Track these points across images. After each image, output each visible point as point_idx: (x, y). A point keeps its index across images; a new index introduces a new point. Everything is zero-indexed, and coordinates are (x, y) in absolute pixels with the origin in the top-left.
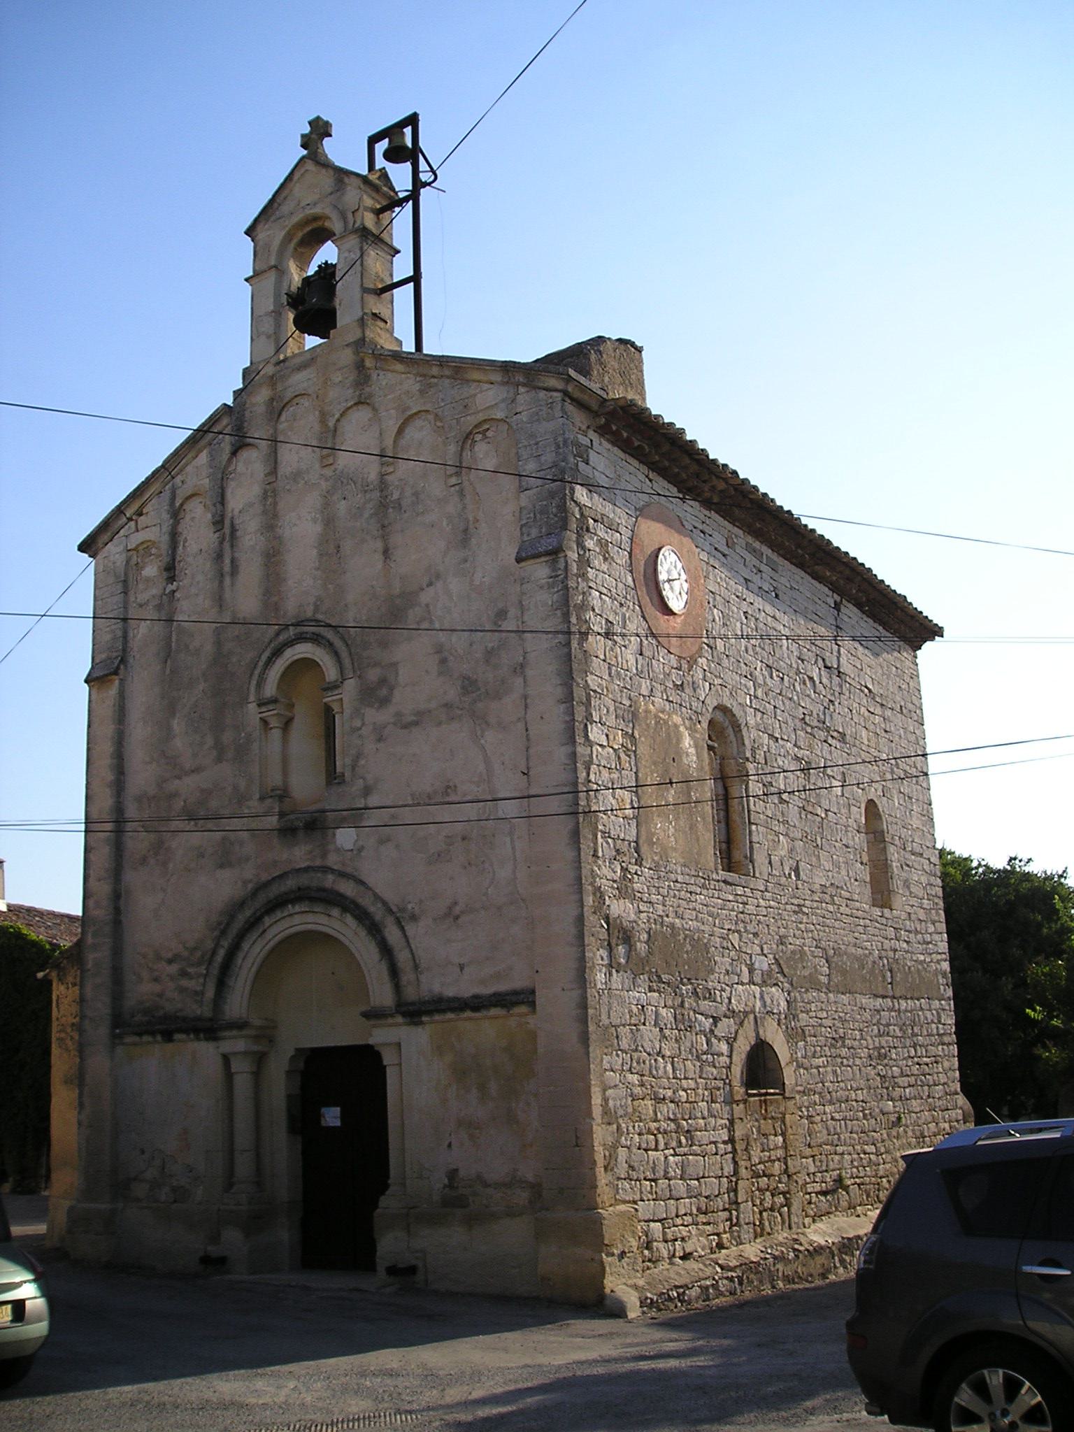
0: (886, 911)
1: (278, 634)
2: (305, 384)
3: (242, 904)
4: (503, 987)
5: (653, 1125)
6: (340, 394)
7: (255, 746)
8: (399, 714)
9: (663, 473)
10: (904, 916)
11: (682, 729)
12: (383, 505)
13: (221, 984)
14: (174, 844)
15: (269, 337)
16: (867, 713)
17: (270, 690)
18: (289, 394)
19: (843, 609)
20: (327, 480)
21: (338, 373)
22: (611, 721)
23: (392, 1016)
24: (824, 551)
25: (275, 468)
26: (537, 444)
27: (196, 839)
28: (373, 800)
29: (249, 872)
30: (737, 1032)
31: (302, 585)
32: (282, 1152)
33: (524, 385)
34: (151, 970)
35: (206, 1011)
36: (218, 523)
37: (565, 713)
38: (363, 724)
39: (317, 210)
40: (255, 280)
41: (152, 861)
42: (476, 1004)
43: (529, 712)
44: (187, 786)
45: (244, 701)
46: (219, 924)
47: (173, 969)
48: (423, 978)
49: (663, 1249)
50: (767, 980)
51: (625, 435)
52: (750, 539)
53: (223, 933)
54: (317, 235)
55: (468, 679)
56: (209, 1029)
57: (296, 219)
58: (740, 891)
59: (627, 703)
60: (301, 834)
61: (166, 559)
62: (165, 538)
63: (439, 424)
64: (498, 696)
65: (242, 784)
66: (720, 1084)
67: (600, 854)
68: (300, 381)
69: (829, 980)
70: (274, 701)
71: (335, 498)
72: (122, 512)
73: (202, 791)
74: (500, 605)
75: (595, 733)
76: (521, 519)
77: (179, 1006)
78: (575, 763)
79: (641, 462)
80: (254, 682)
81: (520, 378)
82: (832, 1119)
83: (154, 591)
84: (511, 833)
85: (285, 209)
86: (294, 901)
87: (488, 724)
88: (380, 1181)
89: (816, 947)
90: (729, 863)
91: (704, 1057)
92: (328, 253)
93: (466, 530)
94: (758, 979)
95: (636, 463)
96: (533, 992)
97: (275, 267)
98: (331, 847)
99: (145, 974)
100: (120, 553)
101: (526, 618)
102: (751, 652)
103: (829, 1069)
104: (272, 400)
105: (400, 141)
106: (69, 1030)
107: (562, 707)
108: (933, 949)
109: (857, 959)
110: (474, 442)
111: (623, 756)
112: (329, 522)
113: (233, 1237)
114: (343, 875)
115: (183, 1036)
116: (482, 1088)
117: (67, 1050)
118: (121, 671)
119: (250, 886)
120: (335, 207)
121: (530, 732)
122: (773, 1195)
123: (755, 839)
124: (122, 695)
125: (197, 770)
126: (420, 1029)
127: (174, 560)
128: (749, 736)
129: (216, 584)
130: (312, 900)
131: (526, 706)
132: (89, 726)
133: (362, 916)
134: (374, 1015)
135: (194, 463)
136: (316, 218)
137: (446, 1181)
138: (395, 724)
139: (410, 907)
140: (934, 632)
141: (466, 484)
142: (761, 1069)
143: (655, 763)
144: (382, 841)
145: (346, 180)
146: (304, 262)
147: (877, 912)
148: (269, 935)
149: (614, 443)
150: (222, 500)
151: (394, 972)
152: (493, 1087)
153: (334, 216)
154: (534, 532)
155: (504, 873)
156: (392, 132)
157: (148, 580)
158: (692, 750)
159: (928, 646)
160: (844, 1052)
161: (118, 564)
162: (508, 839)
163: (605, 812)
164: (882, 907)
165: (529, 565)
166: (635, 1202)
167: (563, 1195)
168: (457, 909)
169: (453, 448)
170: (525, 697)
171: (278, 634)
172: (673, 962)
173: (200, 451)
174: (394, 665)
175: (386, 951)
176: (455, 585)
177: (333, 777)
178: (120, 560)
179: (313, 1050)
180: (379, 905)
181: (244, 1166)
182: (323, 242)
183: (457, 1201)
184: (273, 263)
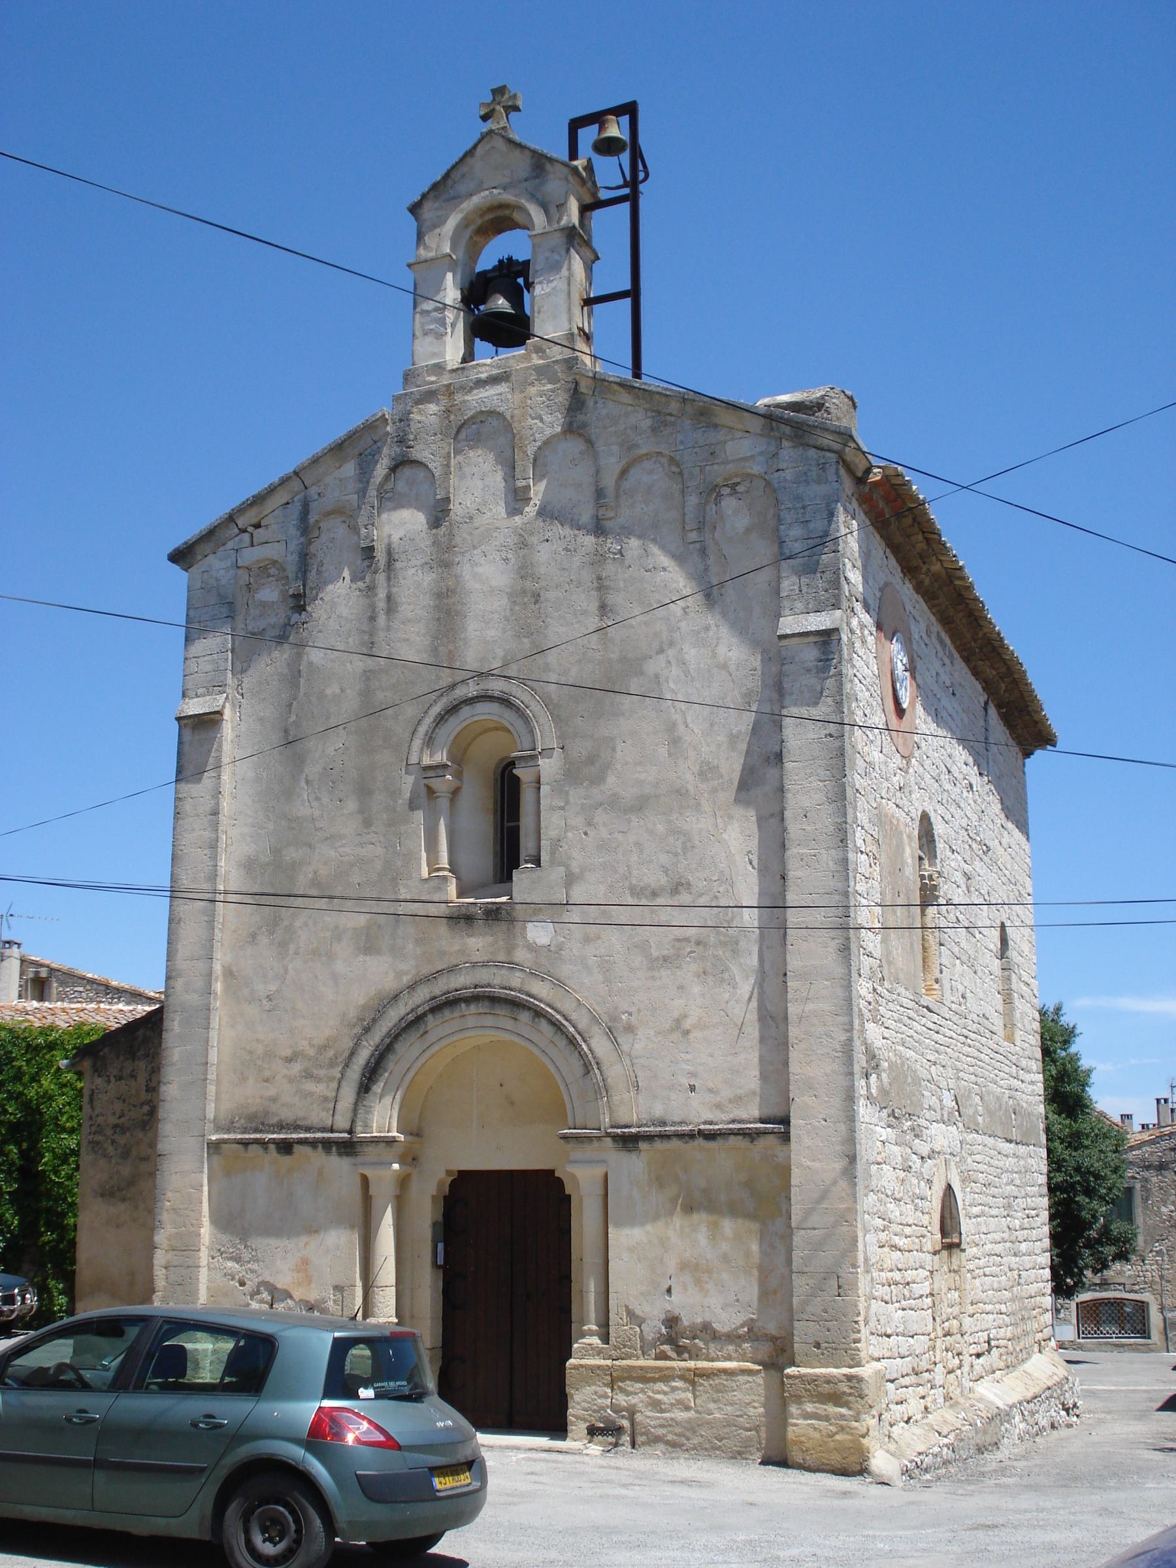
26: (804, 508)
28: (578, 894)
77: (301, 1114)
83: (273, 620)
100: (227, 569)
106: (109, 1132)
110: (720, 495)
126: (634, 1156)
144: (587, 940)
145: (548, 167)
157: (264, 605)
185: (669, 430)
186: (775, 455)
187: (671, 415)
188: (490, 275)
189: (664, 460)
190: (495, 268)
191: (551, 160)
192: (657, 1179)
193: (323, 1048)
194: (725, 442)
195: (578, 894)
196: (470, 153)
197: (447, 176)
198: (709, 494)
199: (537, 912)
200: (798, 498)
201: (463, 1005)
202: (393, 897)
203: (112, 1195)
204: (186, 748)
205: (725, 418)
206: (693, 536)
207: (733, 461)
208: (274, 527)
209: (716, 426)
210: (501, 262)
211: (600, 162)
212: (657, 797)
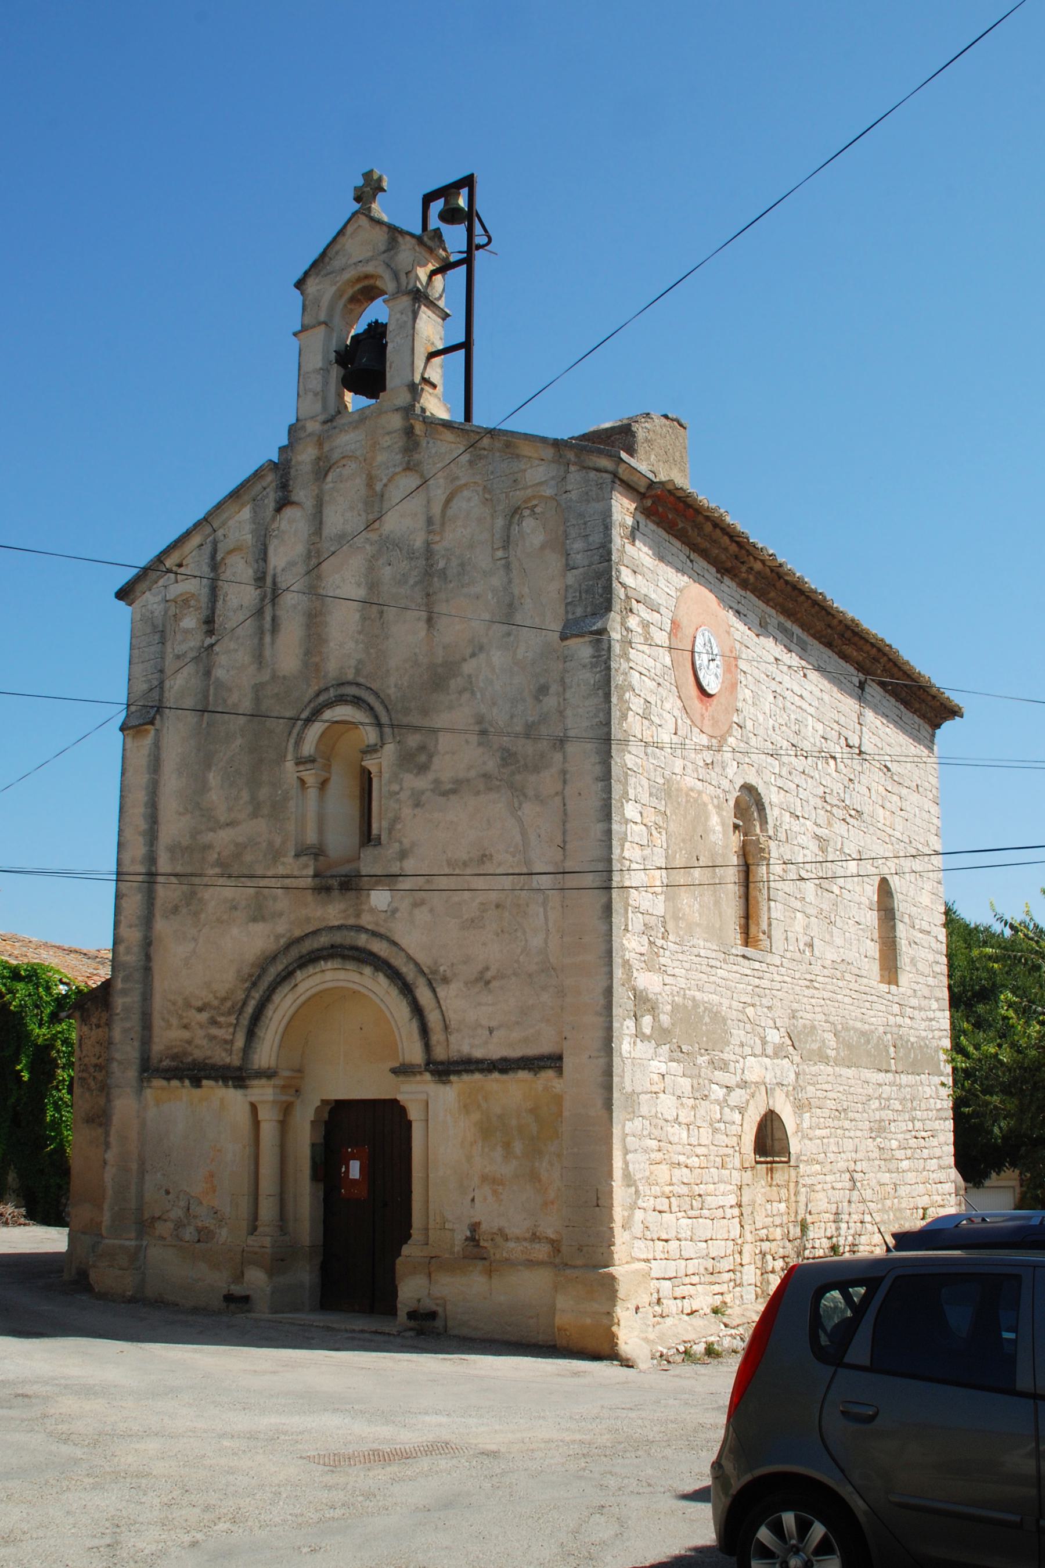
0: (893, 988)
1: (318, 695)
2: (353, 447)
3: (274, 958)
4: (531, 1051)
5: (667, 1189)
6: (388, 457)
7: (292, 804)
8: (437, 782)
9: (704, 554)
10: (910, 992)
11: (710, 807)
12: (428, 573)
13: (251, 1034)
14: (207, 896)
15: (316, 394)
16: (884, 793)
17: (308, 748)
18: (336, 455)
19: (867, 689)
20: (371, 544)
21: (387, 438)
22: (645, 798)
23: (420, 1073)
24: (853, 631)
25: (320, 529)
26: (585, 523)
27: (228, 893)
28: (410, 865)
29: (282, 927)
30: (748, 1101)
31: (344, 645)
32: (305, 1195)
33: (575, 464)
34: (181, 1017)
35: (236, 1062)
36: (260, 579)
37: (602, 790)
38: (401, 789)
39: (369, 269)
40: (303, 335)
41: (184, 910)
42: (504, 1066)
43: (567, 788)
44: (222, 839)
45: (282, 758)
46: (251, 975)
47: (204, 1017)
48: (452, 1039)
49: (671, 1306)
50: (778, 1052)
51: (670, 516)
52: (782, 619)
53: (254, 984)
54: (368, 293)
55: (508, 751)
56: (237, 1077)
57: (347, 275)
58: (757, 965)
59: (661, 781)
60: (336, 893)
61: (205, 613)
62: (205, 591)
63: (487, 496)
64: (536, 770)
65: (278, 841)
66: (730, 1151)
67: (630, 928)
68: (347, 440)
69: (838, 1053)
70: (312, 760)
71: (380, 562)
72: (162, 562)
73: (237, 845)
74: (542, 681)
75: (631, 811)
76: (566, 598)
77: (209, 1053)
78: (610, 839)
79: (683, 543)
80: (292, 741)
81: (571, 456)
82: (833, 1188)
83: (192, 644)
84: (545, 904)
85: (337, 263)
86: (326, 958)
87: (525, 796)
88: (404, 1235)
89: (826, 1022)
90: (748, 938)
91: (717, 1125)
92: (377, 311)
93: (511, 605)
94: (770, 1051)
95: (678, 544)
96: (560, 1058)
97: (325, 323)
98: (365, 907)
99: (174, 1021)
100: (158, 603)
101: (568, 695)
102: (777, 731)
103: (832, 1140)
104: (319, 459)
105: (454, 200)
106: (92, 1070)
107: (600, 784)
108: (933, 1022)
109: (863, 1034)
110: (522, 517)
111: (654, 832)
112: (373, 586)
113: (256, 1279)
114: (375, 934)
115: (211, 1083)
116: (507, 1146)
117: (89, 1089)
118: (157, 722)
119: (282, 941)
120: (388, 266)
121: (568, 807)
122: (774, 1259)
123: (773, 915)
124: (157, 745)
125: (230, 824)
126: (448, 1088)
127: (213, 613)
128: (772, 814)
129: (256, 641)
130: (344, 957)
131: (565, 782)
132: (123, 774)
133: (395, 975)
134: (403, 1071)
135: (237, 518)
136: (367, 277)
137: (468, 1234)
138: (433, 791)
139: (442, 969)
140: (952, 712)
141: (512, 559)
142: (769, 1141)
143: (683, 841)
144: (416, 905)
145: (400, 239)
146: (352, 317)
147: (884, 987)
148: (301, 989)
149: (658, 524)
150: (263, 555)
151: (424, 1031)
152: (518, 1147)
153: (387, 276)
154: (579, 611)
155: (536, 942)
156: (447, 192)
157: (186, 631)
158: (718, 828)
159: (947, 725)
160: (847, 1124)
161: (156, 614)
162: (541, 910)
163: (636, 888)
164: (889, 983)
165: (572, 642)
166: (648, 1261)
167: (582, 1252)
168: (489, 975)
169: (500, 522)
170: (564, 772)
171: (318, 695)
172: (693, 1035)
173: (243, 505)
174: (434, 731)
175: (417, 1010)
176: (498, 657)
177: (367, 838)
178: (158, 609)
179: (337, 1102)
180: (412, 966)
181: (267, 1210)
182: (372, 299)
183: (477, 1249)
184: (322, 317)
185: (483, 462)
186: (564, 479)
187: (485, 449)
188: (361, 338)
189: (480, 489)
190: (365, 331)
191: (403, 233)
192: (465, 1106)
193: (224, 1000)
194: (525, 470)
195: (410, 865)
196: (341, 232)
197: (324, 254)
198: (512, 516)
199: (377, 883)
200: (581, 515)
201: (322, 962)
202: (525, 871)
203: (93, 1121)
204: (128, 754)
205: (526, 449)
206: (500, 554)
207: (531, 486)
208: (192, 565)
209: (518, 456)
210: (369, 325)
211: (447, 230)
212: (468, 780)
